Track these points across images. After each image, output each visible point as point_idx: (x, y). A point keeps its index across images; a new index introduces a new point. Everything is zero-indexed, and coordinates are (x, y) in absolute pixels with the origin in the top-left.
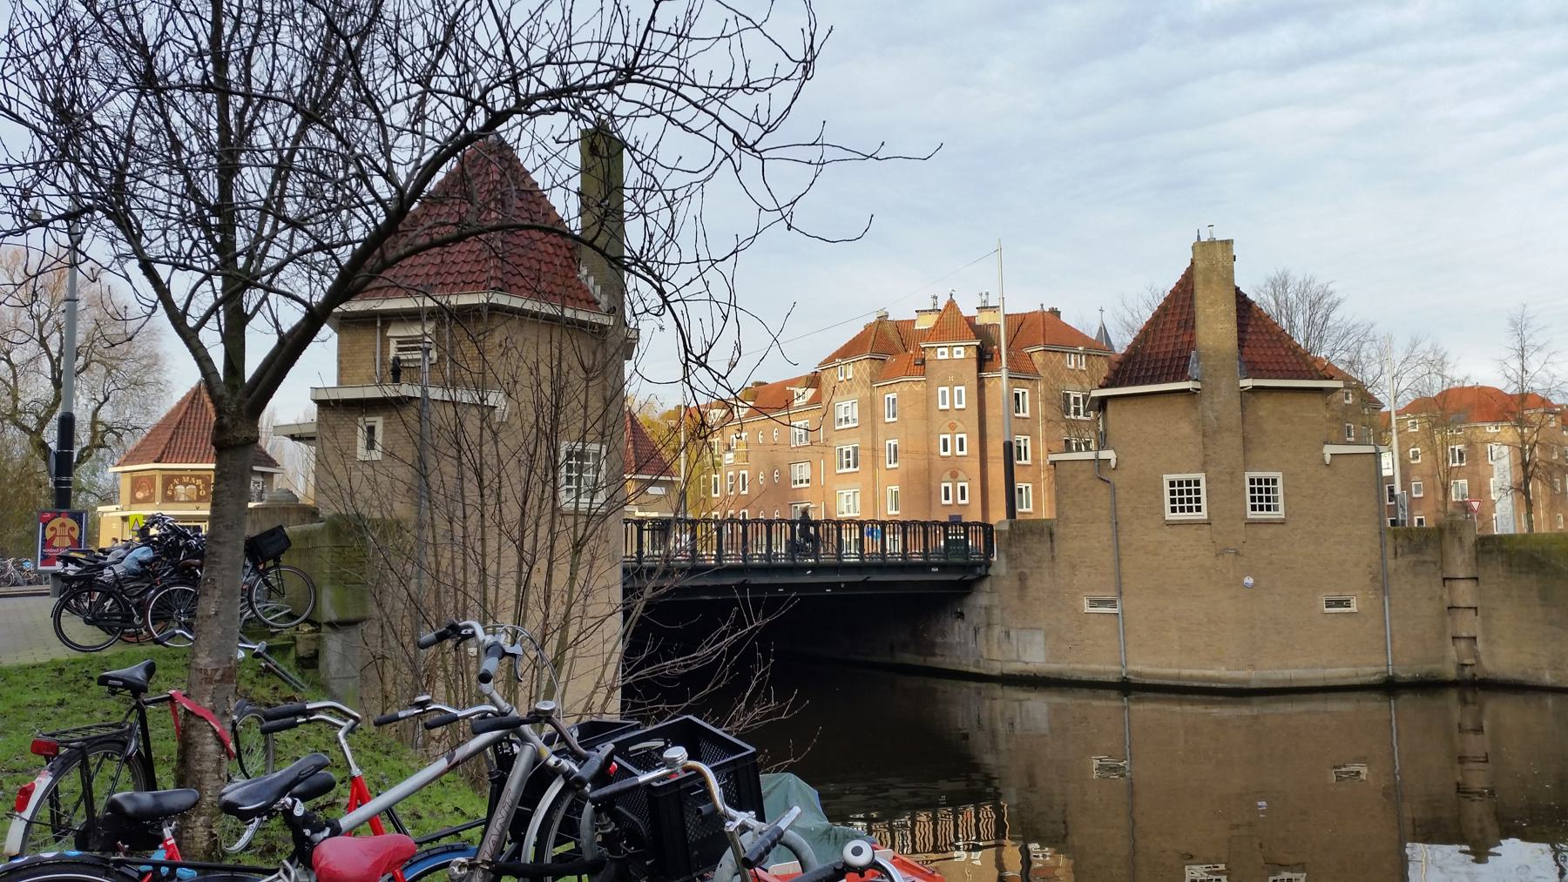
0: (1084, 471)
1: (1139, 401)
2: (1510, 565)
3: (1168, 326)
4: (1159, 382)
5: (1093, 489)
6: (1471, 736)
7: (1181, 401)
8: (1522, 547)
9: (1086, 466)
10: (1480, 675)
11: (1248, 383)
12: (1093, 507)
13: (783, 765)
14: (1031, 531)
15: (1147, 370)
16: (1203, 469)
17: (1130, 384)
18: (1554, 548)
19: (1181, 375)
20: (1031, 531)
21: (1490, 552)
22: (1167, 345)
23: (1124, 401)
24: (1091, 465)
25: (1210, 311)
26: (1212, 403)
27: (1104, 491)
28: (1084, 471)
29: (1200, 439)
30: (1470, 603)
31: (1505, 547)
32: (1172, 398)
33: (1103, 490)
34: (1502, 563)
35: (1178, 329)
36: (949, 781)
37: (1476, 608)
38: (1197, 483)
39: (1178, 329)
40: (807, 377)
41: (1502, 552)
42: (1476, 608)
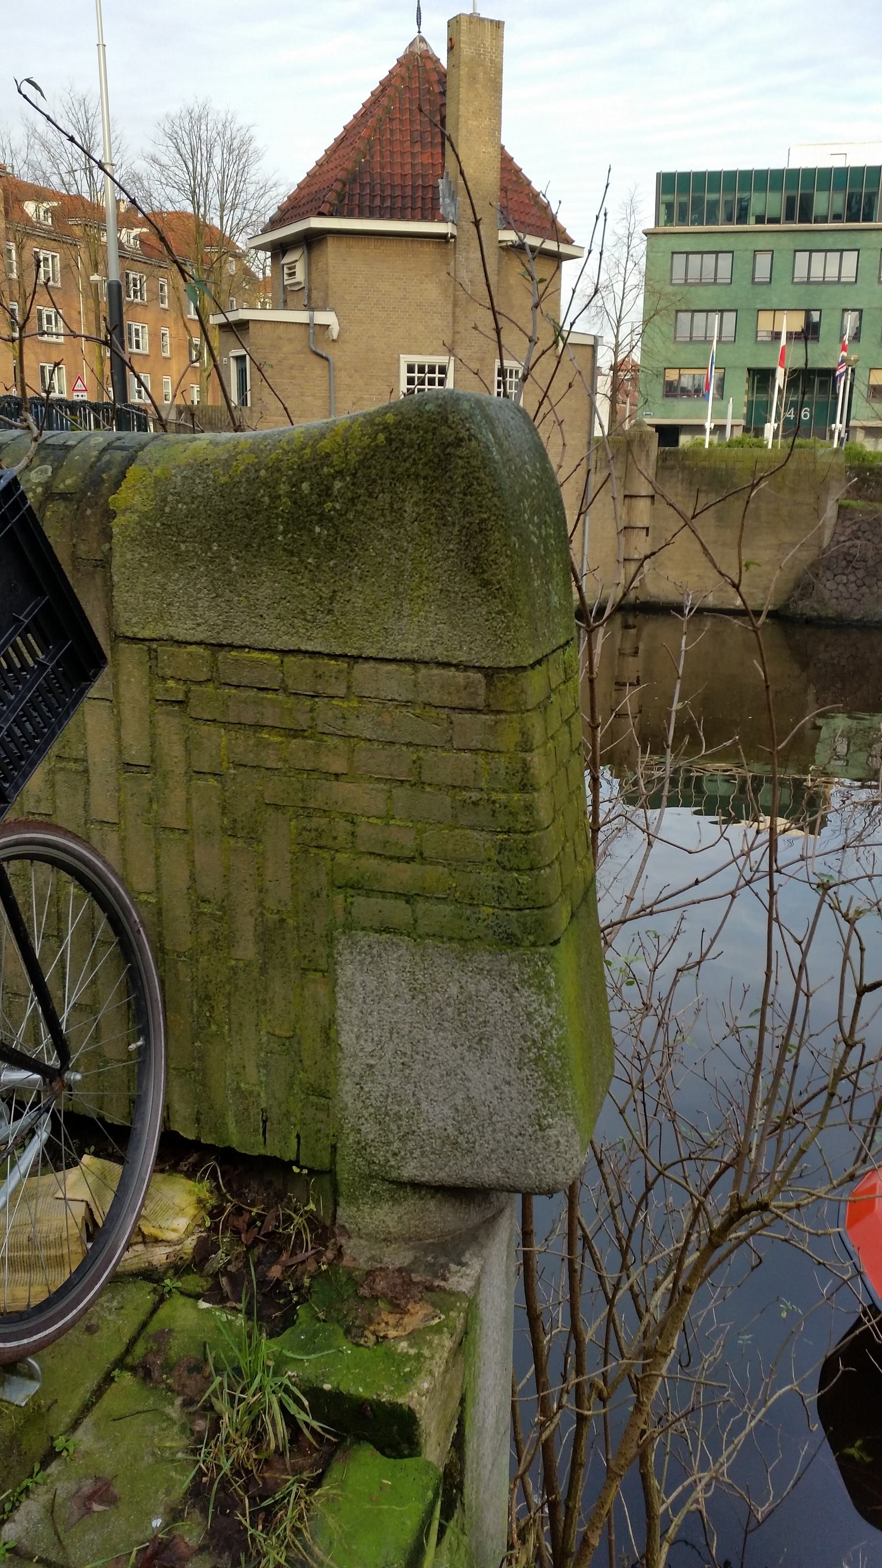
0: (290, 340)
1: (372, 242)
2: (691, 484)
3: (398, 136)
4: (403, 218)
5: (302, 368)
6: (631, 659)
7: (428, 250)
8: (706, 464)
9: (295, 332)
10: (642, 598)
11: (509, 236)
12: (302, 394)
13: (699, 723)
14: (210, 423)
15: (383, 199)
16: (451, 352)
17: (361, 215)
18: (739, 465)
19: (431, 213)
20: (210, 423)
21: (672, 468)
22: (402, 165)
23: (351, 242)
24: (301, 331)
25: (473, 123)
26: (467, 259)
27: (319, 372)
28: (290, 340)
29: (449, 308)
30: (646, 523)
31: (687, 463)
32: (416, 245)
33: (317, 369)
34: (683, 481)
35: (413, 143)
36: (849, 717)
37: (647, 529)
38: (443, 370)
39: (413, 143)
40: (427, 51)
41: (684, 468)
42: (647, 529)
